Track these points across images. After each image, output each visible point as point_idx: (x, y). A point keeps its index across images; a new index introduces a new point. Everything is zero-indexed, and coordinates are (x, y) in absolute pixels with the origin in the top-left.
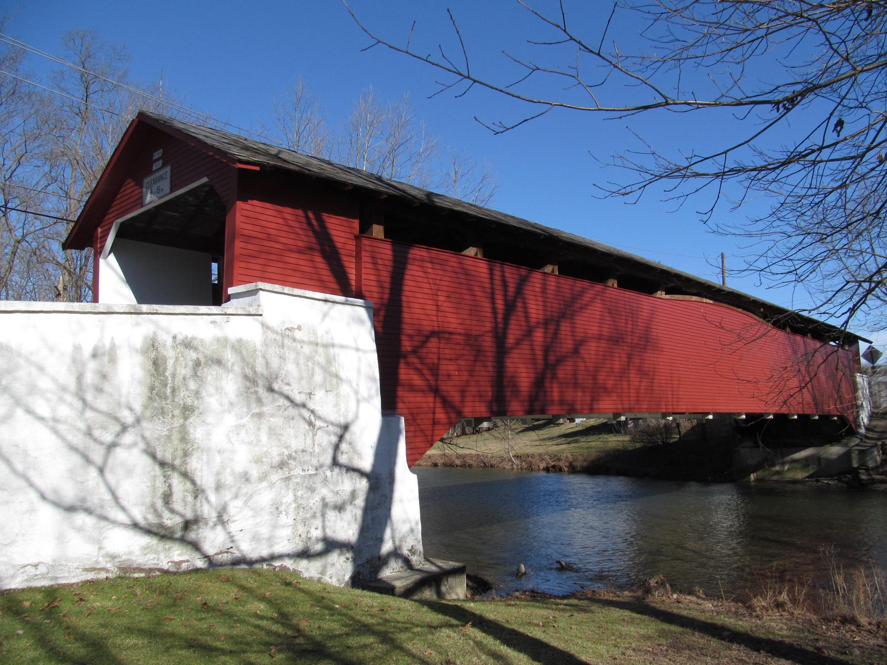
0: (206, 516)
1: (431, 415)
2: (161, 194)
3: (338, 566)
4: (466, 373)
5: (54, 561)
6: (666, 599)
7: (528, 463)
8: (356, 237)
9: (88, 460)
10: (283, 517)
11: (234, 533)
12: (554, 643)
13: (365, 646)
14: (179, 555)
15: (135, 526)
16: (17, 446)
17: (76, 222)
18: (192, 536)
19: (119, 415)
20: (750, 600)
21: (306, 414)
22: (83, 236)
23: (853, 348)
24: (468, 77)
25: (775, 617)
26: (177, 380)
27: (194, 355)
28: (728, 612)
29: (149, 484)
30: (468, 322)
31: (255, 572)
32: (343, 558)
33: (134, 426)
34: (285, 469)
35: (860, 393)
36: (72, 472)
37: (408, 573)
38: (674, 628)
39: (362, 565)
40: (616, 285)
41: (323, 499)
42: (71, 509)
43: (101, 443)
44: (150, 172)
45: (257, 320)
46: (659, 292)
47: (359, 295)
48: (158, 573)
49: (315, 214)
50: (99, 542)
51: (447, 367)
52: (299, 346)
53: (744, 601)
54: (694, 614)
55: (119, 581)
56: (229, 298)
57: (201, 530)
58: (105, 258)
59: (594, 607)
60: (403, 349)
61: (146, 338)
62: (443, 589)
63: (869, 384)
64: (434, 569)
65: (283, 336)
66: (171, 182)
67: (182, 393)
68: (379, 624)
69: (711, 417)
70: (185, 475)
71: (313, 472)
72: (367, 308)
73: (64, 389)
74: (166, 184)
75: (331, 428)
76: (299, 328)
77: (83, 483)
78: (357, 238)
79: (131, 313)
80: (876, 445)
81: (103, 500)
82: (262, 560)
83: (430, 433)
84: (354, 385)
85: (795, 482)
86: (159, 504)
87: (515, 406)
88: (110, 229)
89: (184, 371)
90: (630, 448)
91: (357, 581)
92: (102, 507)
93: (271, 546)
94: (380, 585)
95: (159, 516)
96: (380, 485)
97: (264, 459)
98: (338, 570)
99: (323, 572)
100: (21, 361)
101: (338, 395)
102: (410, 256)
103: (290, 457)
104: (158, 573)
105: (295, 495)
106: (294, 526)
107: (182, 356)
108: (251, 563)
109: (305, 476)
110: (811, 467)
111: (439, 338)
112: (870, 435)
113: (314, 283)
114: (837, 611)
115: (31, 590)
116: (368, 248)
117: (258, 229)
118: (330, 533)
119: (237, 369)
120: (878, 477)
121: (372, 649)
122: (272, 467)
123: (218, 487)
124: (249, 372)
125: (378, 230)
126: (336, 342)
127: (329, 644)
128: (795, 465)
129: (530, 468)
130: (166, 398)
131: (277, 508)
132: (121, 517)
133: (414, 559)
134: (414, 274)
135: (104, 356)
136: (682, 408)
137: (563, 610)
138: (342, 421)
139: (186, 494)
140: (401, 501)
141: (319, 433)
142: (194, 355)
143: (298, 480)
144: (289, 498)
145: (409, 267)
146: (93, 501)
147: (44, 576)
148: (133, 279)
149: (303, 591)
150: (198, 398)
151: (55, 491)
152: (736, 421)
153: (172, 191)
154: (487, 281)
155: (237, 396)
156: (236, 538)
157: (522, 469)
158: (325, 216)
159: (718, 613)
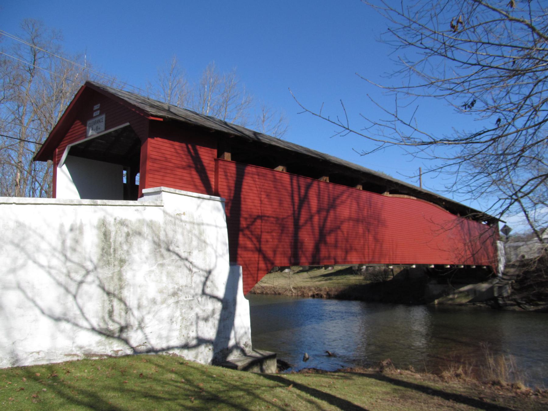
0: (132, 324)
1: (256, 265)
2: (99, 131)
3: (205, 354)
4: (276, 241)
5: (48, 350)
6: (390, 372)
7: (302, 292)
8: (215, 159)
9: (67, 290)
10: (174, 324)
11: (147, 334)
12: (339, 396)
13: (239, 397)
14: (117, 347)
15: (93, 329)
16: (28, 282)
17: (43, 145)
18: (124, 335)
19: (85, 265)
20: (442, 372)
21: (188, 264)
22: (47, 153)
23: (495, 226)
24: (348, 129)
25: (455, 381)
26: (116, 244)
27: (125, 230)
28: (429, 379)
29: (101, 305)
30: (278, 210)
31: (160, 356)
32: (207, 349)
33: (92, 271)
34: (176, 297)
35: (499, 253)
36: (59, 298)
37: (244, 358)
38: (400, 388)
39: (218, 353)
40: (361, 189)
41: (197, 314)
42: (58, 320)
43: (75, 281)
44: (92, 117)
45: (161, 209)
46: (386, 193)
47: (217, 194)
48: (106, 357)
49: (192, 146)
50: (72, 339)
51: (265, 236)
52: (184, 224)
53: (437, 372)
54: (411, 381)
55: (85, 362)
56: (142, 195)
57: (129, 333)
58: (61, 167)
59: (354, 377)
60: (241, 226)
61: (99, 220)
62: (264, 367)
63: (504, 247)
64: (258, 355)
65: (175, 218)
66: (106, 124)
67: (119, 252)
68: (242, 386)
69: (414, 266)
70: (121, 300)
71: (192, 298)
72: (222, 202)
73: (55, 249)
74: (102, 125)
75: (201, 273)
76: (184, 214)
77: (64, 304)
78: (216, 160)
79: (91, 205)
80: (507, 284)
81: (75, 314)
82: (163, 350)
83: (256, 275)
84: (214, 247)
85: (461, 305)
86: (107, 317)
87: (303, 260)
88: (64, 150)
89: (121, 239)
90: (364, 284)
91: (216, 362)
92: (75, 318)
93: (168, 341)
94: (228, 365)
95: (106, 324)
96: (228, 306)
97: (164, 291)
98: (204, 356)
99: (196, 357)
100: (31, 232)
101: (205, 253)
102: (246, 171)
103: (179, 289)
104: (106, 357)
105: (181, 312)
106: (180, 330)
107: (120, 230)
108: (156, 351)
109: (186, 301)
110: (470, 296)
111: (262, 220)
112: (505, 277)
113: (191, 187)
114: (489, 378)
115: (37, 366)
116: (222, 167)
117: (160, 155)
118: (201, 335)
119: (150, 238)
120: (509, 302)
121: (244, 398)
122: (169, 296)
123: (139, 307)
124: (156, 239)
125: (227, 156)
126: (205, 222)
127: (221, 395)
128: (461, 295)
129: (303, 296)
130: (110, 255)
131: (171, 320)
132: (85, 324)
133: (248, 350)
134: (248, 182)
135: (77, 230)
136: (398, 261)
137: (337, 378)
138: (208, 268)
139: (121, 311)
140: (240, 315)
141: (195, 275)
142: (125, 230)
143: (183, 303)
144: (178, 314)
145: (246, 178)
146: (71, 315)
147: (43, 359)
148: (77, 180)
149: (192, 367)
150: (128, 255)
151: (50, 309)
152: (427, 268)
153: (106, 129)
154: (289, 186)
155: (150, 254)
156: (149, 337)
157: (298, 296)
158: (198, 147)
159: (424, 380)
